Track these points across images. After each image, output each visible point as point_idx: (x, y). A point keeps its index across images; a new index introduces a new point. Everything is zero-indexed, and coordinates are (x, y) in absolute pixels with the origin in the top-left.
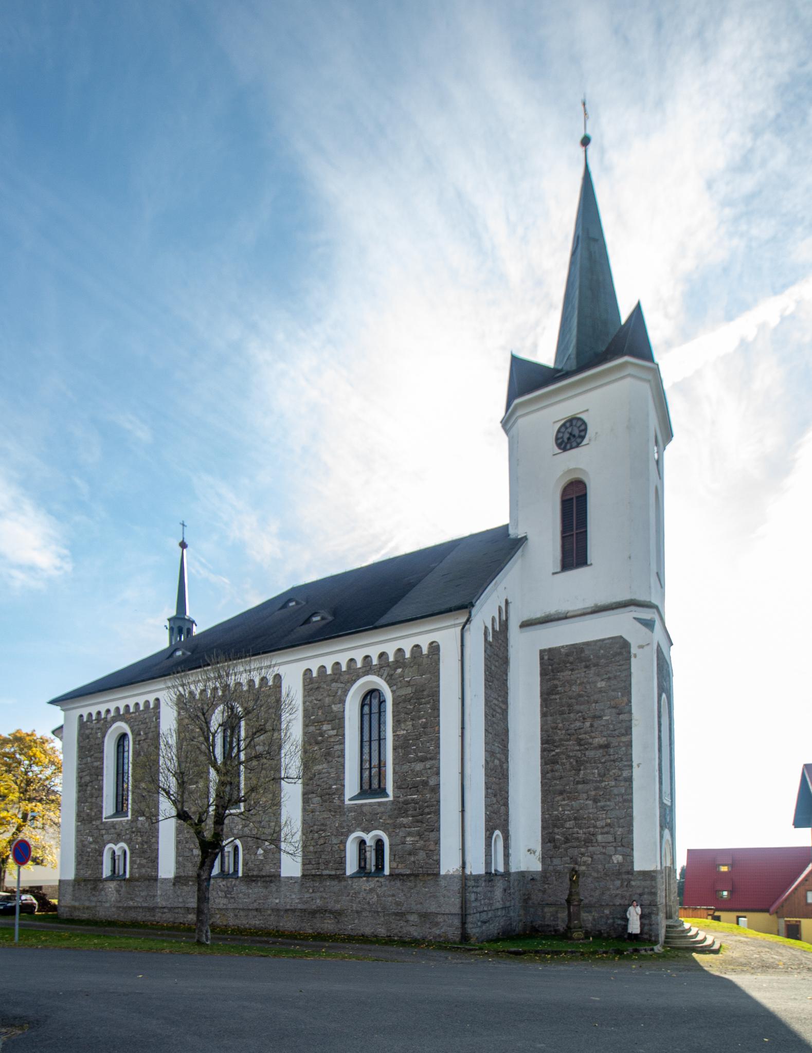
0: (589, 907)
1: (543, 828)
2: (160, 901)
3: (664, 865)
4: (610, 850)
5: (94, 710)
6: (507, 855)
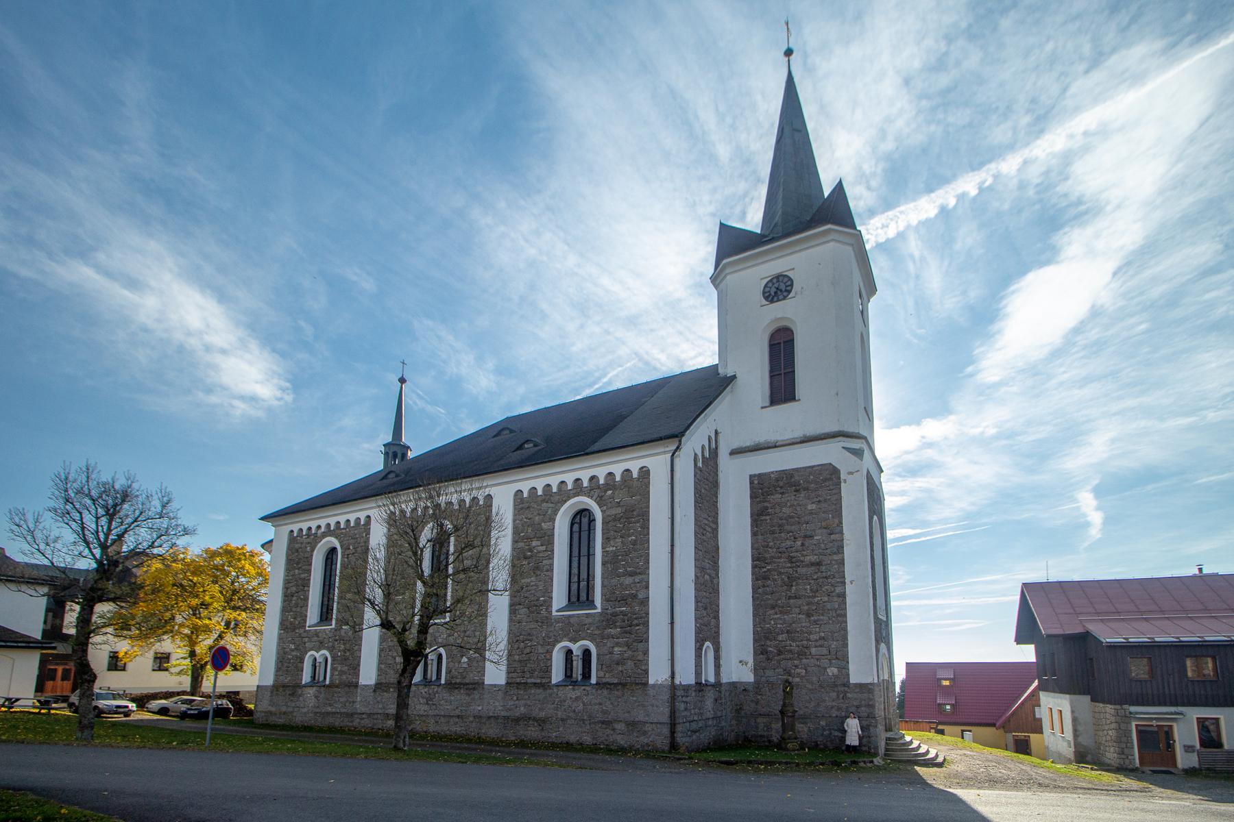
0: (804, 719)
1: (755, 641)
2: (359, 708)
4: (825, 662)
6: (718, 666)
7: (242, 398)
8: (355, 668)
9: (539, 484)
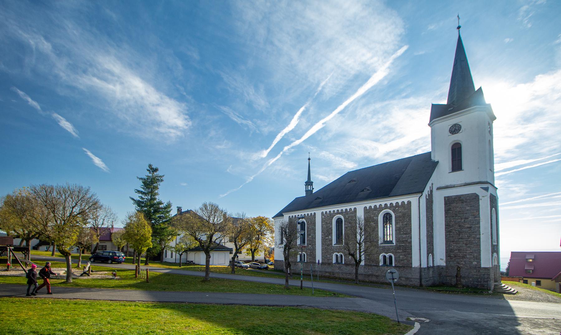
0: (464, 278)
1: (446, 252)
2: (317, 269)
3: (494, 264)
4: (472, 260)
5: (294, 215)
6: (433, 261)
7: (173, 128)
8: (314, 258)
9: (373, 205)
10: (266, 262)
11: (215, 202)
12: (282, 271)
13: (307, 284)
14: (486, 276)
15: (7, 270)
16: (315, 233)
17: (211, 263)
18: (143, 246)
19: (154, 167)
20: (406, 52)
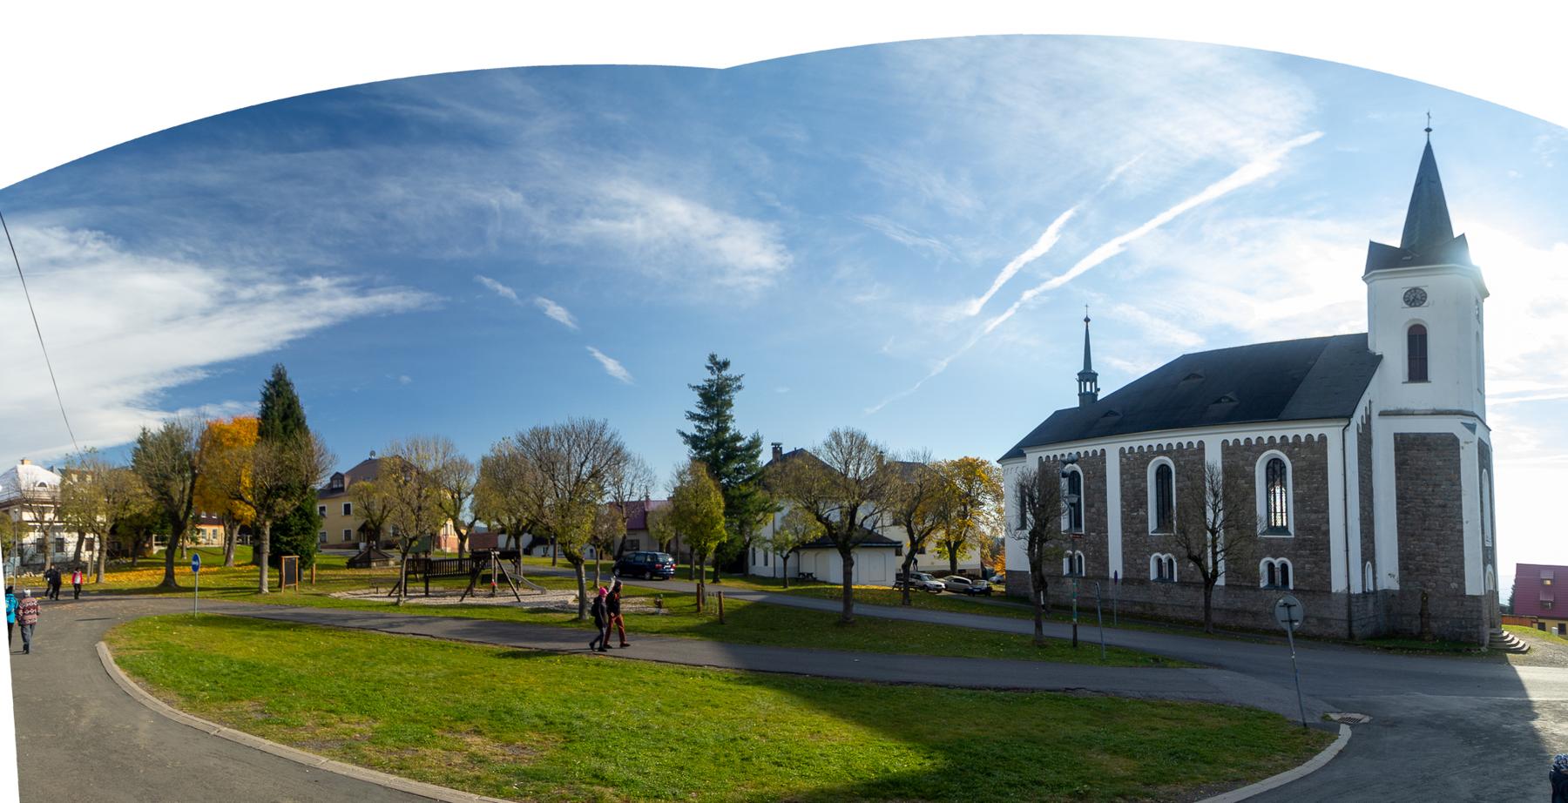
4: (1449, 579)
6: (1375, 579)
8: (1105, 564)
9: (1242, 437)
10: (986, 575)
11: (859, 427)
12: (1024, 599)
13: (1087, 633)
14: (1475, 615)
15: (492, 595)
16: (1105, 502)
17: (854, 579)
18: (709, 538)
19: (720, 359)
20: (1318, 141)
